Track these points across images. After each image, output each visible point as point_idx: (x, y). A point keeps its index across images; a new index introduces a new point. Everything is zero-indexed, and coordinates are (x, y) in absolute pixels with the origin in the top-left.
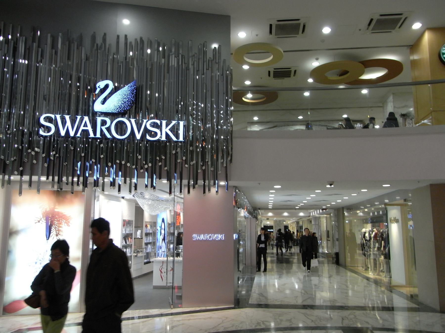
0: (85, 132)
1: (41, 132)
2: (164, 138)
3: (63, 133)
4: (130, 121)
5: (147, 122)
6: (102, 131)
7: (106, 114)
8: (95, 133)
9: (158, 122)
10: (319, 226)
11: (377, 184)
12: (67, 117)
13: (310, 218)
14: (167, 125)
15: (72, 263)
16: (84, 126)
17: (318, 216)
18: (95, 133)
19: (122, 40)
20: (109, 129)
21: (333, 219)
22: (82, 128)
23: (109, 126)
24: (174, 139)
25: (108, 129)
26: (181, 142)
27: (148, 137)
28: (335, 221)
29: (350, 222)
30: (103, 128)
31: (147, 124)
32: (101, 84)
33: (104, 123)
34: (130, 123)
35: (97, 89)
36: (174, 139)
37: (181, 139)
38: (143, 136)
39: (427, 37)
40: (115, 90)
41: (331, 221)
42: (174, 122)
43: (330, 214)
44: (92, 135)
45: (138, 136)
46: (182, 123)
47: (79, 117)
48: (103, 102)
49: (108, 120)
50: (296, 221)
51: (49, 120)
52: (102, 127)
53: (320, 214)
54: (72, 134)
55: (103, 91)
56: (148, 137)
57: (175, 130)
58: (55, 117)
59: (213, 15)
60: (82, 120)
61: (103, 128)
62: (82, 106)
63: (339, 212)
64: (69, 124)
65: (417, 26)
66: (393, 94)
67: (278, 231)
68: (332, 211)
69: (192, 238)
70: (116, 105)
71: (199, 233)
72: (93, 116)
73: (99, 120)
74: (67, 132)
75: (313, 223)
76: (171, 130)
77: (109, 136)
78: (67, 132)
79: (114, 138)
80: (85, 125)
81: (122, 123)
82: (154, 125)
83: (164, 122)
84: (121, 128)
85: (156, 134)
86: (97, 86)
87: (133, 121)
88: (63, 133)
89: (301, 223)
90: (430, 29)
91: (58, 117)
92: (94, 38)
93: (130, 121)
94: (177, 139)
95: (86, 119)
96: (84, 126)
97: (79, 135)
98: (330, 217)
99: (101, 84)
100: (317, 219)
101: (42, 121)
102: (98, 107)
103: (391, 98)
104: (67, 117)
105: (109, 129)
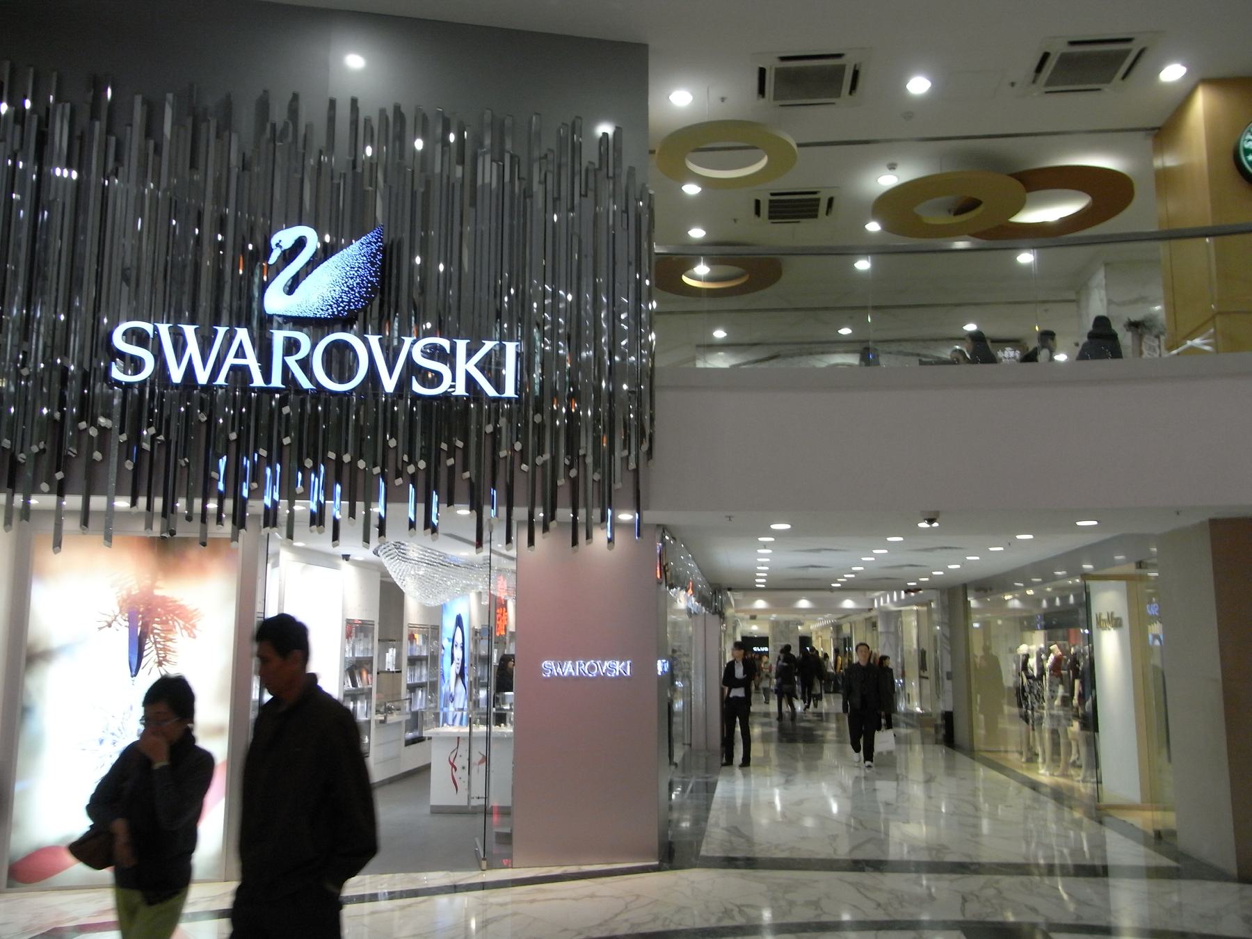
0: (240, 373)
1: (116, 374)
2: (460, 390)
3: (177, 375)
4: (366, 342)
5: (414, 343)
6: (286, 368)
7: (298, 322)
8: (267, 376)
9: (445, 343)
10: (897, 637)
11: (1061, 518)
12: (189, 331)
13: (873, 613)
14: (470, 354)
15: (203, 743)
16: (236, 356)
17: (893, 608)
18: (267, 376)
19: (343, 112)
20: (305, 365)
21: (936, 617)
22: (231, 360)
23: (308, 356)
24: (491, 391)
25: (303, 364)
26: (509, 400)
27: (417, 387)
28: (941, 624)
29: (986, 625)
30: (291, 361)
31: (414, 348)
32: (285, 238)
33: (292, 346)
34: (366, 348)
35: (272, 250)
36: (491, 391)
37: (510, 392)
38: (403, 384)
39: (1201, 103)
40: (325, 253)
41: (932, 623)
42: (489, 345)
43: (928, 604)
44: (258, 381)
45: (389, 384)
46: (511, 348)
47: (222, 331)
48: (291, 288)
49: (304, 338)
50: (833, 624)
51: (138, 337)
52: (288, 359)
53: (901, 602)
54: (202, 377)
55: (289, 255)
56: (417, 387)
57: (491, 366)
58: (156, 329)
59: (599, 41)
60: (230, 337)
61: (291, 361)
62: (230, 298)
63: (953, 597)
64: (193, 348)
65: (1173, 73)
66: (1106, 265)
67: (782, 651)
68: (934, 595)
69: (541, 671)
70: (327, 295)
71: (560, 658)
72: (263, 326)
73: (279, 337)
74: (190, 372)
75: (880, 628)
76: (481, 366)
77: (305, 383)
78: (190, 372)
79: (320, 388)
80: (240, 353)
81: (345, 346)
82: (435, 353)
83: (462, 345)
84: (339, 360)
85: (438, 377)
86: (274, 241)
87: (374, 340)
88: (177, 375)
89: (846, 630)
90: (1209, 81)
91: (164, 329)
92: (263, 106)
93: (366, 342)
94: (498, 391)
95: (242, 334)
96: (236, 356)
97: (221, 380)
98: (930, 611)
99: (285, 238)
100: (892, 618)
101: (118, 342)
102: (276, 301)
103: (1100, 277)
104: (189, 331)
105: (305, 365)
